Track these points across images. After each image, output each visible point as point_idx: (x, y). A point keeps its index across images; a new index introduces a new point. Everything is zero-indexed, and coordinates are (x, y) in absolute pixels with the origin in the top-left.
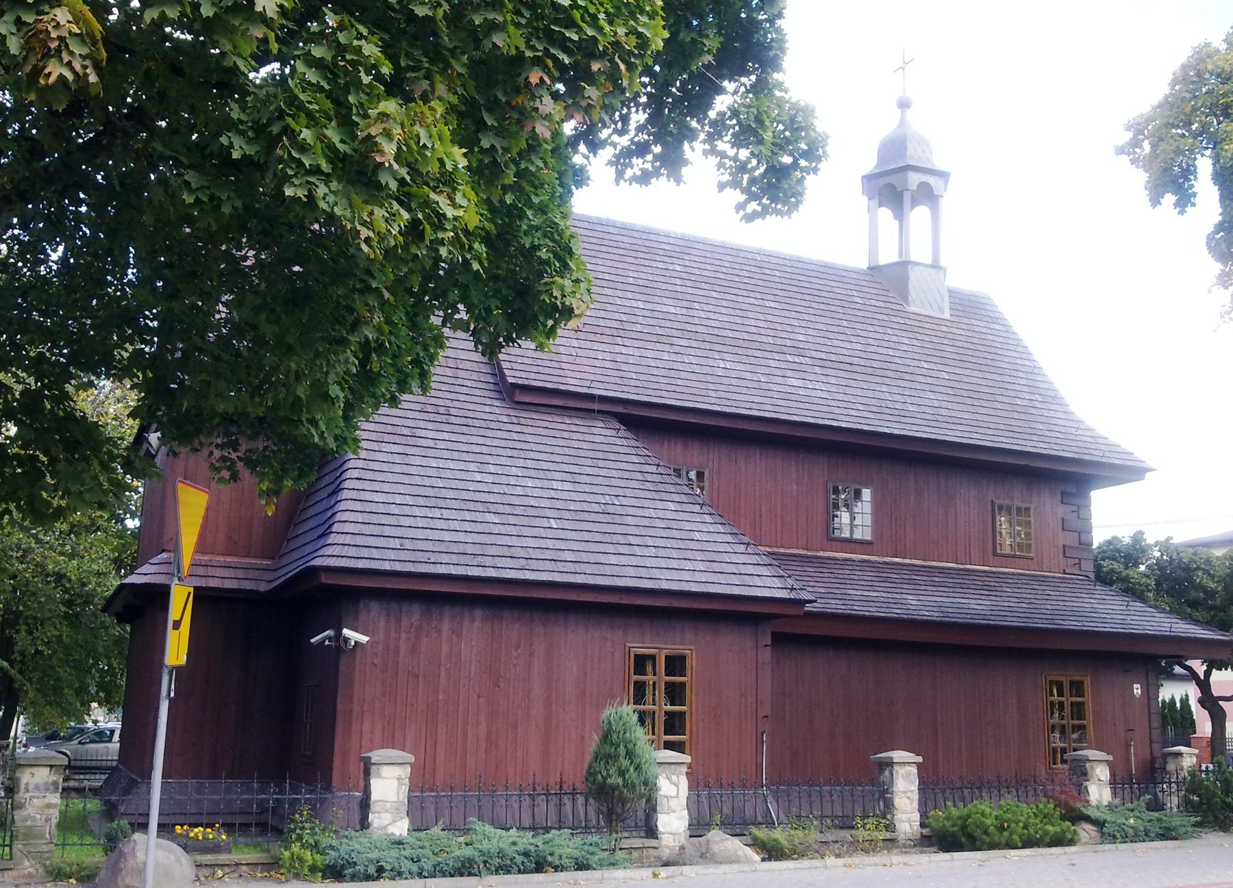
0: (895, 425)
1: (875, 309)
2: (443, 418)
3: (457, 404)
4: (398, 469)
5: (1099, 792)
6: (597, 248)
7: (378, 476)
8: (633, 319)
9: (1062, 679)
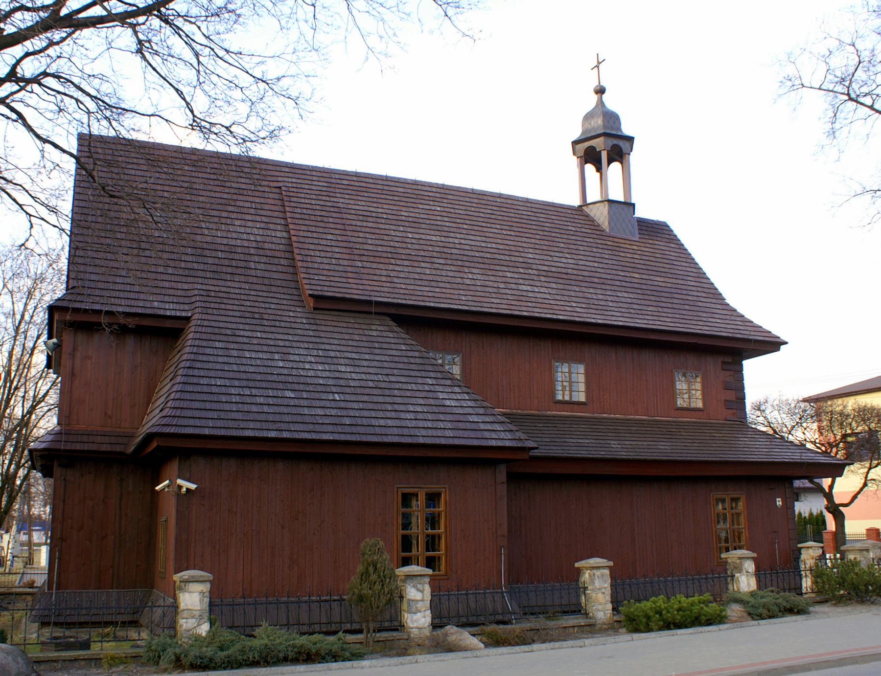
0: (599, 317)
1: (585, 235)
2: (258, 322)
3: (269, 311)
4: (221, 359)
5: (746, 582)
6: (378, 196)
7: (206, 366)
8: (404, 245)
9: (724, 496)
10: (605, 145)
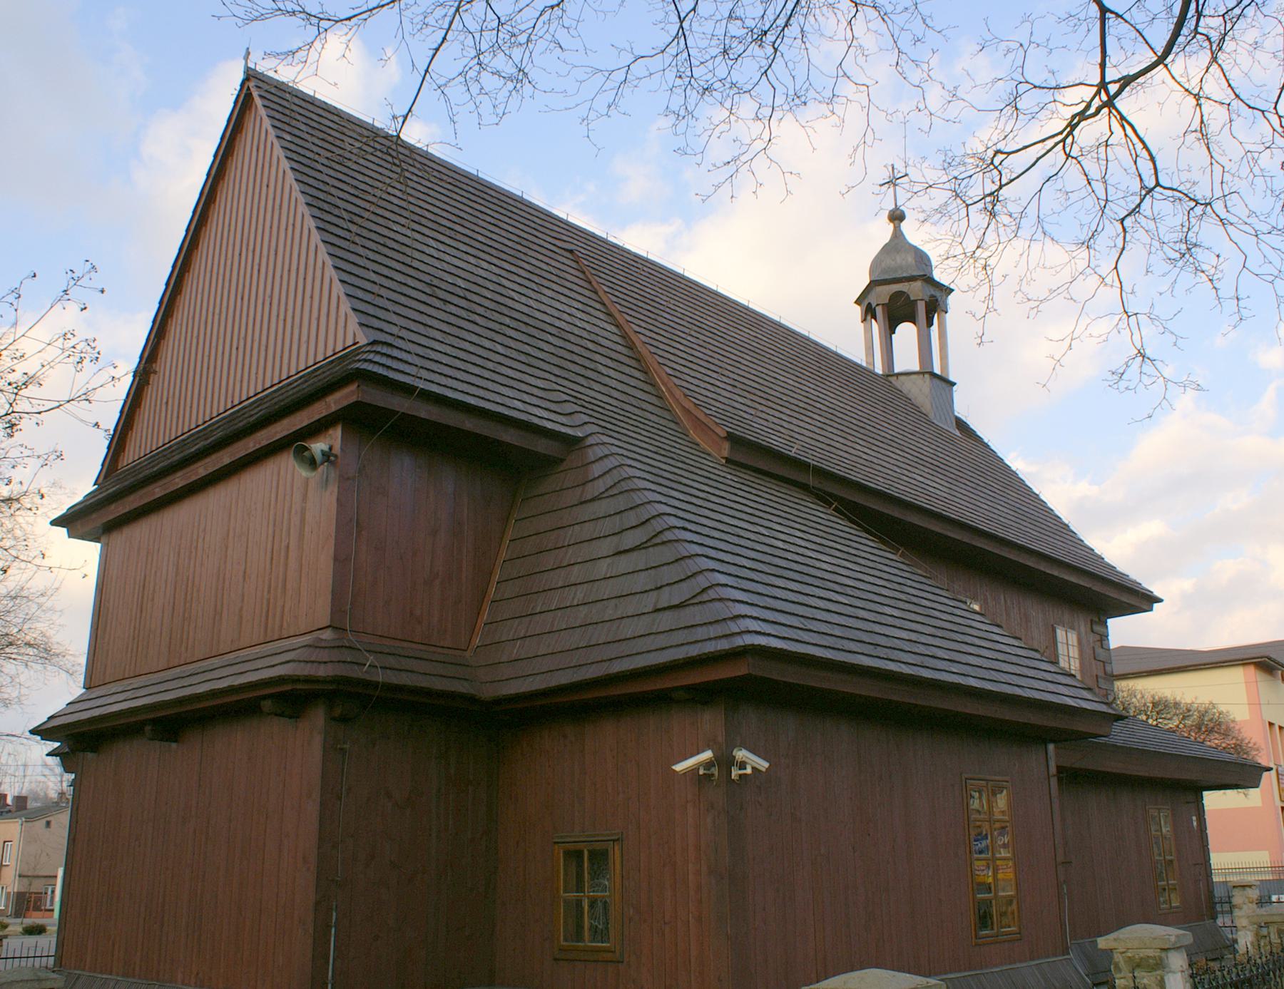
10: (905, 294)
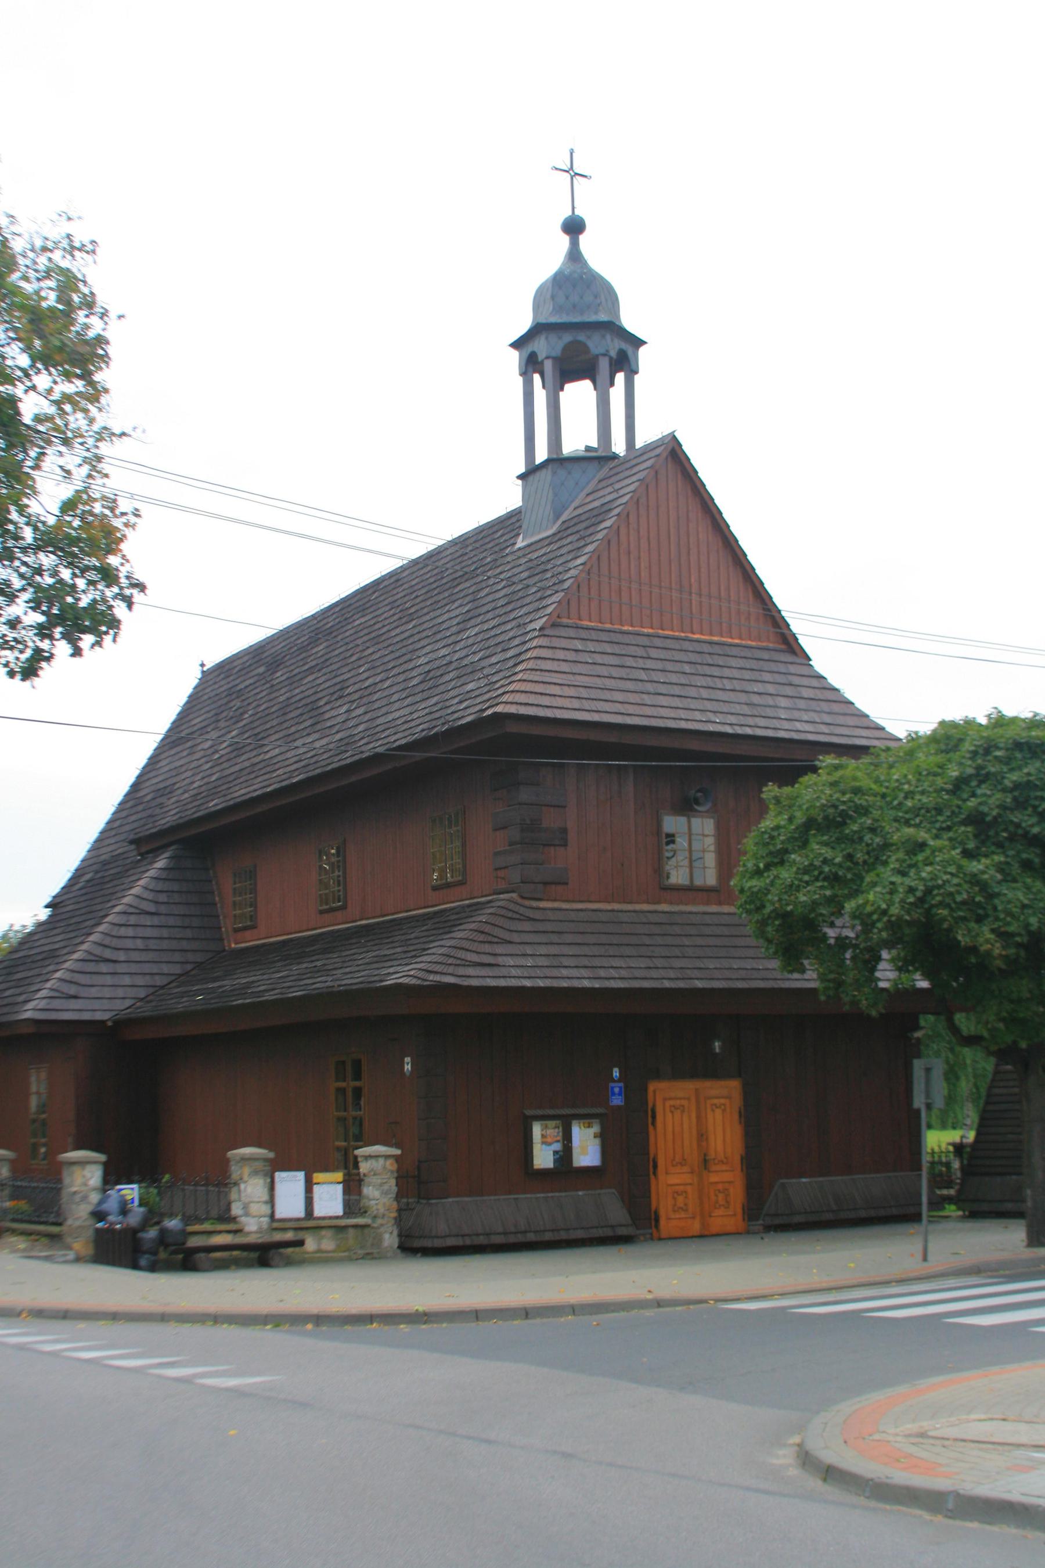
10: (577, 337)
